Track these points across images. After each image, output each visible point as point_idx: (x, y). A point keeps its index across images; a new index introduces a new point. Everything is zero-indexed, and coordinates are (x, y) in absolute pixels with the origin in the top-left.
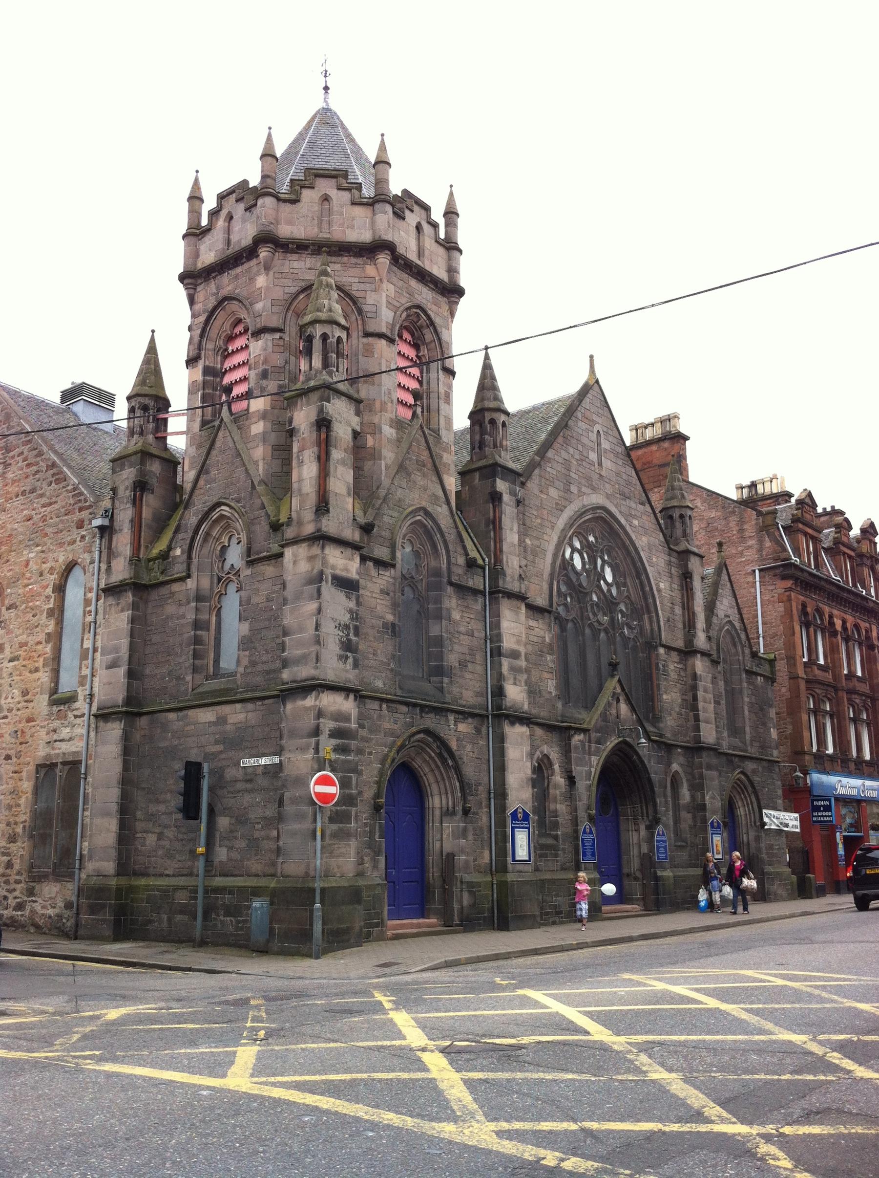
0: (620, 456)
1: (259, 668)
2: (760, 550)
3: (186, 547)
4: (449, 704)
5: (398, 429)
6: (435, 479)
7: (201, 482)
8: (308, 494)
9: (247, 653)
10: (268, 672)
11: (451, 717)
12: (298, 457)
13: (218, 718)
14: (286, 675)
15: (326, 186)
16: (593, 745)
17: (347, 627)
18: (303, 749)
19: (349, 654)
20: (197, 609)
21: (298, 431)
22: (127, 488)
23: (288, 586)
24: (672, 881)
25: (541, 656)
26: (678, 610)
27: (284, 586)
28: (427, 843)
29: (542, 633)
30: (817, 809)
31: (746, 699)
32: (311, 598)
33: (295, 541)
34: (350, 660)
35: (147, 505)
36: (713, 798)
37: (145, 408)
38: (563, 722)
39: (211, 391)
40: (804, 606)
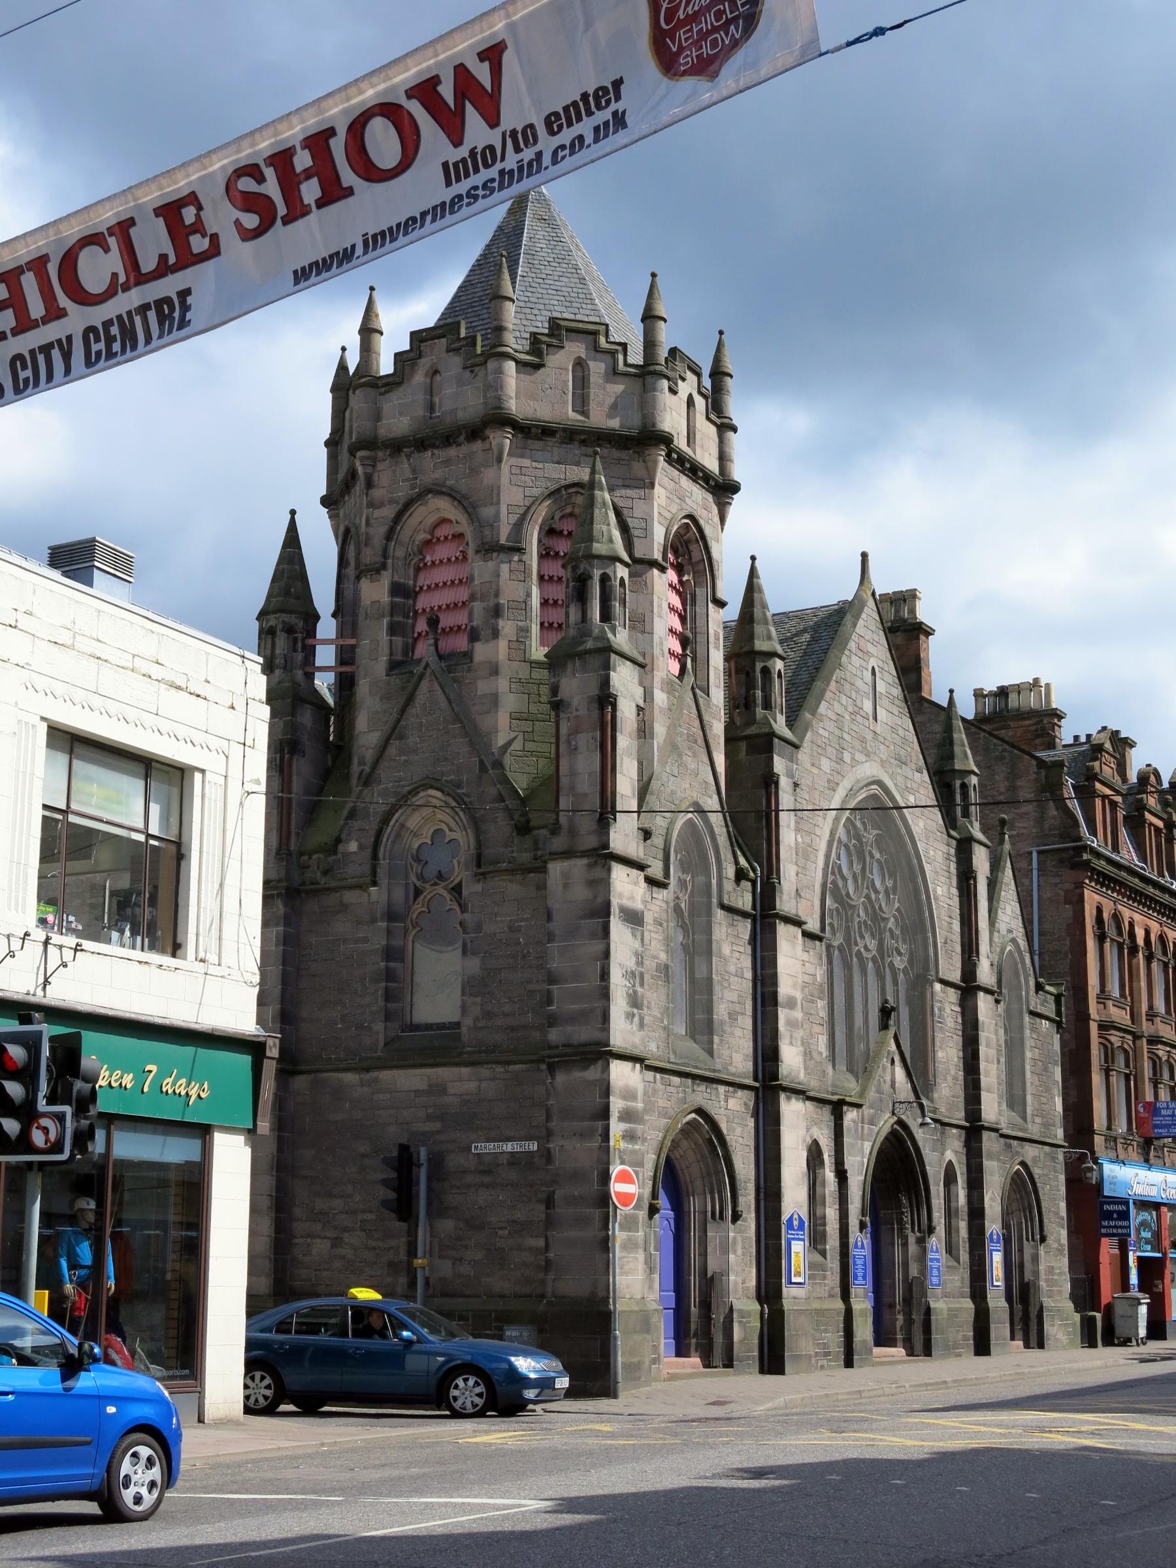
0: (897, 702)
1: (499, 1022)
2: (1041, 820)
4: (719, 1071)
5: (669, 693)
6: (706, 759)
7: (392, 750)
8: (585, 795)
9: (478, 1000)
10: (513, 1029)
11: (722, 1089)
12: (569, 742)
13: (430, 1086)
14: (554, 1036)
15: (575, 349)
16: (866, 1126)
17: (633, 973)
18: (583, 1135)
19: (635, 1011)
20: (389, 932)
21: (569, 705)
23: (556, 917)
24: (945, 1312)
25: (812, 1002)
27: (549, 917)
28: (686, 1257)
29: (812, 971)
30: (1108, 1215)
31: (1028, 1054)
32: (593, 936)
34: (636, 1019)
35: (298, 774)
36: (992, 1199)
37: (290, 630)
38: (833, 1094)
39: (401, 619)
40: (1099, 910)
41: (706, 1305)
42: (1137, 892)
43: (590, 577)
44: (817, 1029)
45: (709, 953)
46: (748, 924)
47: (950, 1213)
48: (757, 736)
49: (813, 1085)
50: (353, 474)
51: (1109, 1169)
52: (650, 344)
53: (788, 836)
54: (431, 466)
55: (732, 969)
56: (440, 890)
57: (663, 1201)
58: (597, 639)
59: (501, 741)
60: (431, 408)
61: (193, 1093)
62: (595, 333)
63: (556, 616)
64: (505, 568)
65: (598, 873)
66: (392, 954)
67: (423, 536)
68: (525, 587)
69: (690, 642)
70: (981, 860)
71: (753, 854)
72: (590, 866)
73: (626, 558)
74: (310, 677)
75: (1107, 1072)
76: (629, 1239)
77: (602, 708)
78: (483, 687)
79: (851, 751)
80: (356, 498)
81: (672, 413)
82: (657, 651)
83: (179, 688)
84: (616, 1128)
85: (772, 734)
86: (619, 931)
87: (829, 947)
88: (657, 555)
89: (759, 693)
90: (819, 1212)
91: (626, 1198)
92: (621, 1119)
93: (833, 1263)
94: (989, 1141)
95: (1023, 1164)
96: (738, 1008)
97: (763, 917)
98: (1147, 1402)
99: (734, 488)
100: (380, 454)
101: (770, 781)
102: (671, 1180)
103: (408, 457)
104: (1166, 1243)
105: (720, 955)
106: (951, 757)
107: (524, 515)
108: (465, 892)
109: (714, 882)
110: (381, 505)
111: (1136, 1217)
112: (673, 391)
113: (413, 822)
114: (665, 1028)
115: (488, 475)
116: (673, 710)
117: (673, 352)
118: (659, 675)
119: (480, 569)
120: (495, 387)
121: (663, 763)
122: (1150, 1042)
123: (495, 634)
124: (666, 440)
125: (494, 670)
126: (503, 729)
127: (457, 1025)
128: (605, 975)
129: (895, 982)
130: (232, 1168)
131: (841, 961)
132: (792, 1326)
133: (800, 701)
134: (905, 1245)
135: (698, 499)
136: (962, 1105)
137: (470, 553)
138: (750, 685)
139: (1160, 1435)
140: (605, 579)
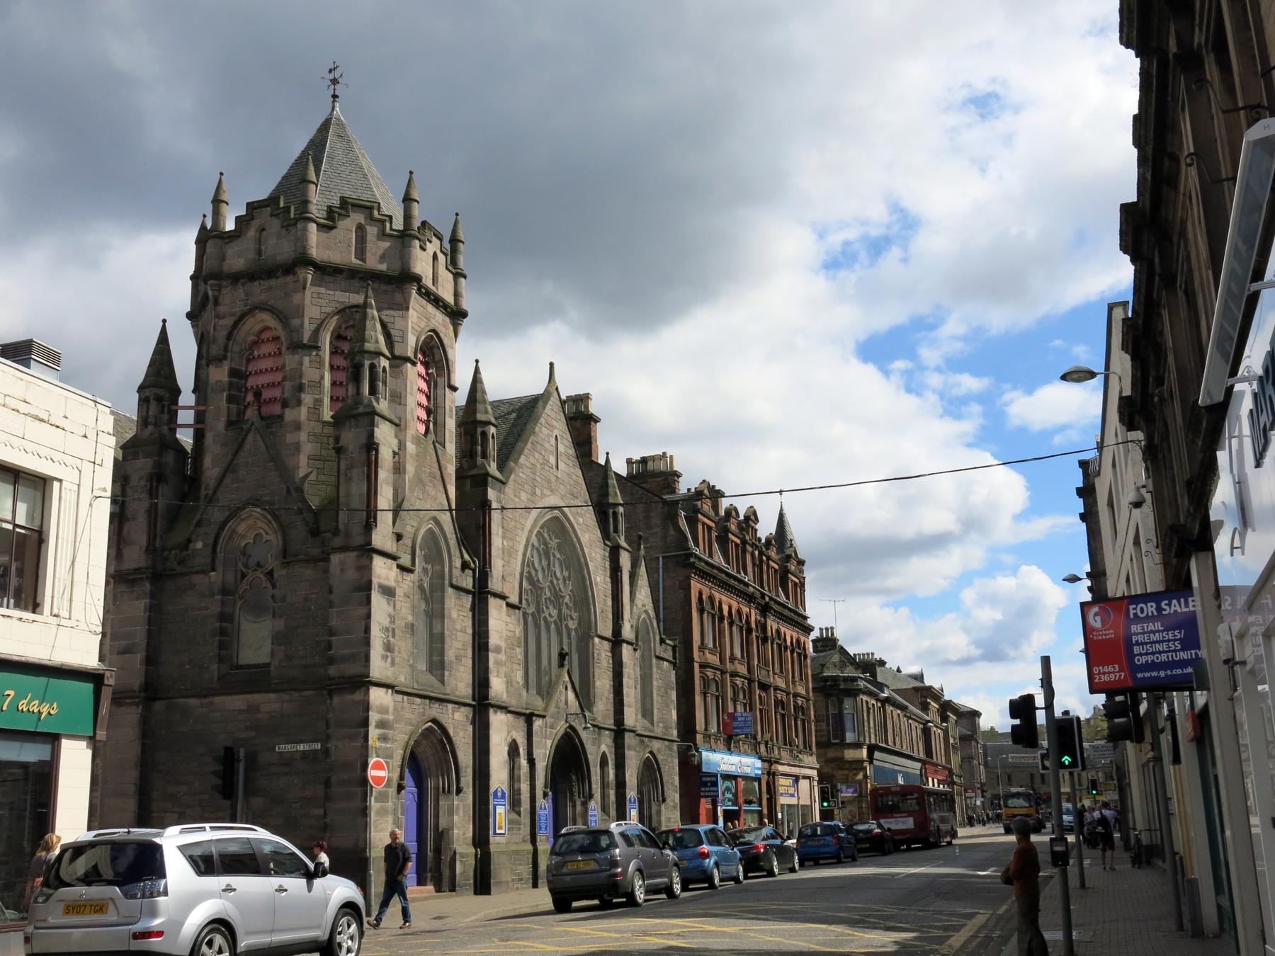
2: (665, 537)
3: (211, 541)
7: (227, 481)
11: (450, 706)
12: (346, 474)
15: (357, 218)
17: (387, 629)
22: (141, 478)
26: (609, 602)
27: (331, 592)
30: (705, 784)
31: (655, 683)
33: (343, 549)
37: (159, 399)
40: (700, 593)
41: (438, 851)
42: (724, 583)
43: (362, 365)
44: (516, 667)
45: (442, 616)
46: (470, 598)
47: (604, 785)
48: (477, 475)
49: (513, 703)
50: (206, 296)
51: (706, 755)
52: (408, 217)
53: (497, 541)
54: (259, 291)
55: (458, 627)
56: (258, 574)
57: (409, 781)
58: (366, 406)
59: (301, 474)
60: (259, 253)
61: (45, 711)
62: (371, 208)
63: (340, 392)
64: (306, 359)
65: (364, 561)
66: (225, 617)
67: (252, 338)
68: (321, 374)
69: (433, 412)
70: (625, 560)
71: (473, 553)
72: (359, 557)
73: (387, 354)
74: (173, 431)
75: (705, 694)
76: (382, 808)
77: (369, 451)
78: (290, 438)
79: (541, 485)
80: (209, 312)
81: (422, 262)
82: (409, 416)
83: (42, 420)
84: (374, 733)
85: (487, 474)
86: (377, 600)
87: (525, 614)
88: (410, 354)
89: (479, 448)
90: (516, 786)
91: (379, 780)
92: (377, 726)
93: (525, 819)
94: (629, 739)
95: (651, 753)
96: (462, 652)
97: (480, 593)
98: (722, 908)
99: (464, 315)
100: (224, 283)
101: (485, 505)
102: (415, 765)
103: (243, 285)
104: (741, 800)
105: (450, 618)
106: (607, 495)
107: (320, 326)
108: (275, 575)
109: (447, 569)
110: (224, 317)
111: (722, 786)
112: (423, 249)
113: (241, 528)
114: (411, 666)
115: (296, 298)
116: (420, 456)
117: (424, 223)
118: (410, 433)
119: (290, 360)
120: (302, 239)
121: (412, 491)
122: (731, 676)
123: (299, 403)
124: (417, 279)
125: (298, 427)
126: (303, 466)
127: (268, 665)
128: (367, 630)
129: (569, 637)
130: (75, 766)
131: (533, 623)
132: (496, 861)
133: (507, 455)
134: (574, 806)
135: (439, 320)
136: (612, 716)
137: (284, 349)
138: (473, 442)
139: (724, 934)
140: (373, 367)
